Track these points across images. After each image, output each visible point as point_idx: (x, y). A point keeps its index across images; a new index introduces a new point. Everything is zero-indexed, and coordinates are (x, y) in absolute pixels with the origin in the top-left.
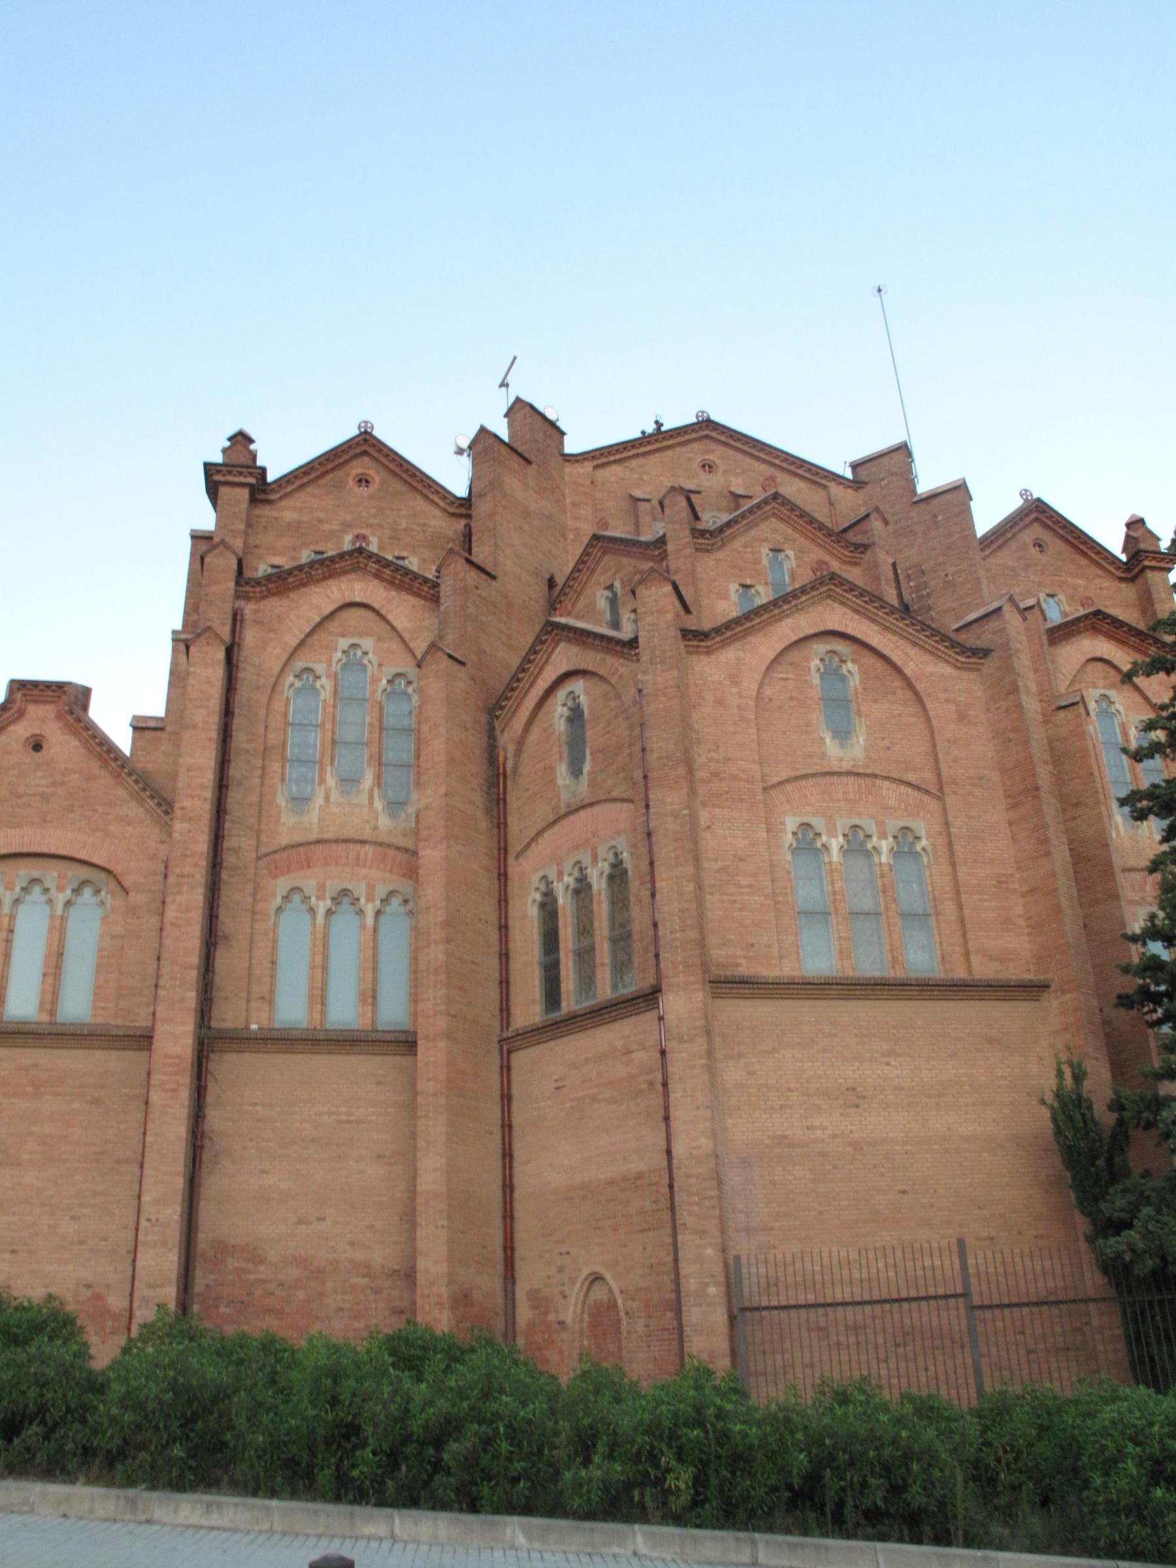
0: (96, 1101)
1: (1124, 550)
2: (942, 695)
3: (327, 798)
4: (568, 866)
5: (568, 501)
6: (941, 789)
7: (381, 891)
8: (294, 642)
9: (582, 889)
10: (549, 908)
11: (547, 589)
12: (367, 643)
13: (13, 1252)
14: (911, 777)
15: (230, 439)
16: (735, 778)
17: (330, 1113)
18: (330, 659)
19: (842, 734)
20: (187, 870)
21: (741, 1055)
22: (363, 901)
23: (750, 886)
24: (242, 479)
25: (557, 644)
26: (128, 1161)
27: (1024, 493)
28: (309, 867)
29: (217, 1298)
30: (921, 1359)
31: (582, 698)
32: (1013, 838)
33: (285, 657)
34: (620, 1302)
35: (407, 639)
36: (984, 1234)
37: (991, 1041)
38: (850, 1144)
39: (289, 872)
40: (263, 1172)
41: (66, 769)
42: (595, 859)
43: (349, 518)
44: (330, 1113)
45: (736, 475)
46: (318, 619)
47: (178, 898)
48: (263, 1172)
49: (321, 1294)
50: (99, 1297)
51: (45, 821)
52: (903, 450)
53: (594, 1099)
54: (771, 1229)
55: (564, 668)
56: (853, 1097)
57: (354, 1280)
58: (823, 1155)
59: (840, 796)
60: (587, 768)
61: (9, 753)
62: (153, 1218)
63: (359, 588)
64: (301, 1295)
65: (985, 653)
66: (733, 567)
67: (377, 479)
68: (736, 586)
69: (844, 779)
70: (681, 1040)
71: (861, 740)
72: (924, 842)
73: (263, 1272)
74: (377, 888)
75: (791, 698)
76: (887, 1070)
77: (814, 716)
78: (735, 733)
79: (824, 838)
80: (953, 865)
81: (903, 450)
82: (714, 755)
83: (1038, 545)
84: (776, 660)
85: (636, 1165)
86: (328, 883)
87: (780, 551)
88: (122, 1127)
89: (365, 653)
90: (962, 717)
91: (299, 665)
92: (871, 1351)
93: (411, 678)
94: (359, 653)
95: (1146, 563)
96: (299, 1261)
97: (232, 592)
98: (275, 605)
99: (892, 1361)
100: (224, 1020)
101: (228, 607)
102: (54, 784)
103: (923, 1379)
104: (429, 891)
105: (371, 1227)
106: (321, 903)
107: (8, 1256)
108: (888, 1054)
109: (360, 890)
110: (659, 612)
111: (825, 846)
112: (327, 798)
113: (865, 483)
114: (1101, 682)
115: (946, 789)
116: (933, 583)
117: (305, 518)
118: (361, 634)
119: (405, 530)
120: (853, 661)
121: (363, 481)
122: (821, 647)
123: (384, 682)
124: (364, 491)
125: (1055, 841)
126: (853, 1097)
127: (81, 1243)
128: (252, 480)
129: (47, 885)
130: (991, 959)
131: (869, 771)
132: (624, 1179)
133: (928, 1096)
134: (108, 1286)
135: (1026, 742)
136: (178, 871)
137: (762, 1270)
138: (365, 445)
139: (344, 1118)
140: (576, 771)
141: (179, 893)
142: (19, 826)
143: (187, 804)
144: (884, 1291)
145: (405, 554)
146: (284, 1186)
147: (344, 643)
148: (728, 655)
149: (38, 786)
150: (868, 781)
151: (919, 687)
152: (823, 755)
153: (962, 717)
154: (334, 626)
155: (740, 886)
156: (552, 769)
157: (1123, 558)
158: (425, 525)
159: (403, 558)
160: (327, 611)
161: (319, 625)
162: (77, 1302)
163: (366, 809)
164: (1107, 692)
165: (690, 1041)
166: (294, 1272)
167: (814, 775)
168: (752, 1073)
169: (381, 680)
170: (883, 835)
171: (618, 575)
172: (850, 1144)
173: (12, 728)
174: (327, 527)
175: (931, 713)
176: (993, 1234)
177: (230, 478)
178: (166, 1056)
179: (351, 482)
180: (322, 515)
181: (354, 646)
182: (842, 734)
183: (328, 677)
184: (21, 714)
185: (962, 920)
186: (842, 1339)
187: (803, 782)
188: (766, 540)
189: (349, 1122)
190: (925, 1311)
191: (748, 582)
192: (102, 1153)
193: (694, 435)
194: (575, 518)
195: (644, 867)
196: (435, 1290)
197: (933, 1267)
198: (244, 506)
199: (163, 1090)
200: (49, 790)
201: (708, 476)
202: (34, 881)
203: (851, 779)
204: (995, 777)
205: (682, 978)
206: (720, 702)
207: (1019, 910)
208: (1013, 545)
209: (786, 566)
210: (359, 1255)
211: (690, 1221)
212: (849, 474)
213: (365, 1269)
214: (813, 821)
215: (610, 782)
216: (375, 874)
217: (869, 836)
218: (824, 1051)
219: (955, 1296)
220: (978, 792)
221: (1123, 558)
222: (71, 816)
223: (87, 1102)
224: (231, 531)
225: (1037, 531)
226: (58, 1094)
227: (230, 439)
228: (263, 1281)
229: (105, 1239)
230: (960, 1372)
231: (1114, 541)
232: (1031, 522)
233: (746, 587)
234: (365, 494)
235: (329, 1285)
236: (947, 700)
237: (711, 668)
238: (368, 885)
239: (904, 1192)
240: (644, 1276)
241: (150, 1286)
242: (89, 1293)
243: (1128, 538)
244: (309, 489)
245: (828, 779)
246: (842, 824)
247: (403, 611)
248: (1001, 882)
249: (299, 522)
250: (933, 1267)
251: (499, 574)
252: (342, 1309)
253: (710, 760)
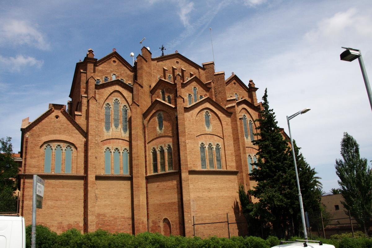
0: (74, 188)
1: (248, 86)
2: (224, 120)
3: (113, 130)
4: (159, 146)
5: (152, 69)
6: (223, 137)
7: (123, 148)
8: (106, 98)
9: (162, 152)
10: (155, 153)
11: (149, 88)
12: (119, 99)
13: (62, 216)
14: (219, 135)
15: (322, 245)
16: (192, 135)
17: (117, 190)
18: (112, 101)
19: (208, 127)
20: (92, 145)
21: (193, 183)
22: (120, 150)
23: (194, 154)
24: (93, 61)
25: (158, 103)
26: (81, 199)
27: (233, 73)
28: (110, 143)
29: (99, 223)
30: (218, 231)
31: (162, 115)
32: (234, 146)
33: (104, 101)
34: (171, 223)
35: (126, 98)
36: (227, 211)
37: (229, 180)
38: (209, 198)
39: (106, 144)
40: (105, 201)
41: (64, 123)
42: (165, 146)
43: (112, 70)
44: (117, 190)
45: (182, 65)
46: (110, 93)
47: (91, 151)
48: (105, 201)
49: (116, 222)
50: (78, 224)
51: (60, 133)
52: (213, 64)
53: (166, 189)
54: (197, 211)
55: (159, 109)
56: (209, 190)
57: (122, 219)
58: (205, 199)
59: (208, 138)
60: (163, 128)
61: (52, 119)
62: (90, 210)
63: (117, 88)
64: (113, 222)
65: (232, 113)
66: (187, 90)
67: (117, 61)
68: (188, 94)
69: (208, 135)
70: (185, 181)
71: (211, 128)
72: (220, 146)
73: (106, 219)
74: (122, 148)
75: (201, 120)
76: (214, 185)
77: (204, 123)
78: (192, 126)
79: (205, 145)
80: (225, 151)
81: (213, 64)
82: (188, 130)
83: (234, 83)
84: (198, 113)
85: (173, 201)
86: (114, 147)
87: (196, 87)
88: (80, 193)
89: (118, 101)
90: (227, 124)
91: (106, 103)
92: (211, 230)
93: (127, 106)
94: (117, 101)
95: (253, 89)
96: (112, 217)
97: (94, 87)
98: (102, 90)
99: (214, 231)
100: (97, 173)
101: (94, 91)
102: (61, 126)
103: (218, 234)
104: (135, 150)
105: (124, 210)
106: (113, 151)
107: (61, 217)
108: (215, 183)
109: (119, 148)
110: (181, 104)
111: (205, 147)
112: (113, 130)
113: (206, 69)
114: (244, 112)
115: (224, 137)
116: (217, 91)
117: (103, 69)
118: (117, 97)
119: (123, 73)
120: (210, 113)
121: (114, 62)
122: (206, 111)
123: (122, 107)
124: (115, 64)
125: (241, 147)
126: (209, 190)
127: (74, 214)
128: (94, 61)
129: (61, 146)
130: (230, 167)
131: (212, 134)
132: (172, 203)
133: (220, 189)
134: (79, 222)
135: (238, 130)
136: (90, 146)
137: (196, 218)
138: (115, 55)
139: (119, 191)
140: (161, 129)
141: (91, 150)
142: (55, 134)
143: (91, 132)
144: (224, 224)
145: (123, 78)
146: (109, 203)
147: (115, 98)
148: (191, 112)
149: (58, 126)
150: (212, 135)
151: (221, 119)
152: (205, 131)
153: (227, 124)
154: (112, 95)
155: (192, 154)
156: (156, 128)
157: (248, 87)
158: (126, 72)
159: (122, 79)
160: (111, 92)
161: (110, 95)
162: (74, 225)
163: (120, 133)
164: (245, 114)
165: (186, 181)
166: (112, 218)
167: (204, 134)
168: (194, 186)
169: (121, 106)
170: (214, 145)
171: (165, 88)
172: (209, 198)
173: (52, 114)
174: (108, 71)
175: (222, 123)
176: (229, 211)
177: (90, 61)
178: (91, 181)
179: (112, 62)
180: (107, 69)
181: (117, 99)
182: (208, 127)
183: (112, 105)
184: (53, 111)
185: (226, 160)
186: (207, 228)
187: (202, 135)
188: (193, 85)
189: (120, 192)
190: (212, 221)
191: (190, 93)
192: (76, 198)
193: (175, 56)
194: (154, 72)
195: (176, 149)
196: (138, 221)
197: (220, 217)
198: (93, 67)
199: (91, 187)
200: (61, 127)
201: (178, 65)
202: (59, 145)
203: (209, 135)
204: (232, 135)
205: (185, 171)
206: (189, 120)
207: (234, 159)
208: (231, 83)
209: (197, 90)
210: (122, 215)
211: (186, 210)
212: (202, 67)
213: (123, 217)
214: (204, 142)
215: (168, 132)
216: (122, 145)
217: (212, 145)
218: (205, 182)
219: (230, 223)
220: (229, 138)
221: (248, 87)
222: (65, 132)
223: (73, 188)
224: (91, 72)
225: (234, 81)
226: (67, 187)
227: (322, 245)
228: (107, 220)
229: (78, 214)
230: (224, 232)
231: (247, 84)
232: (234, 80)
233: (189, 94)
234: (115, 65)
235: (118, 220)
236: (225, 121)
237: (188, 114)
238: (121, 147)
239: (216, 205)
240: (176, 219)
241: (91, 222)
242: (76, 223)
243: (249, 84)
244: (104, 63)
245: (206, 135)
246: (208, 144)
247: (126, 93)
248: (232, 154)
249: (103, 70)
250: (220, 217)
251: (143, 86)
252: (120, 225)
253: (188, 131)
